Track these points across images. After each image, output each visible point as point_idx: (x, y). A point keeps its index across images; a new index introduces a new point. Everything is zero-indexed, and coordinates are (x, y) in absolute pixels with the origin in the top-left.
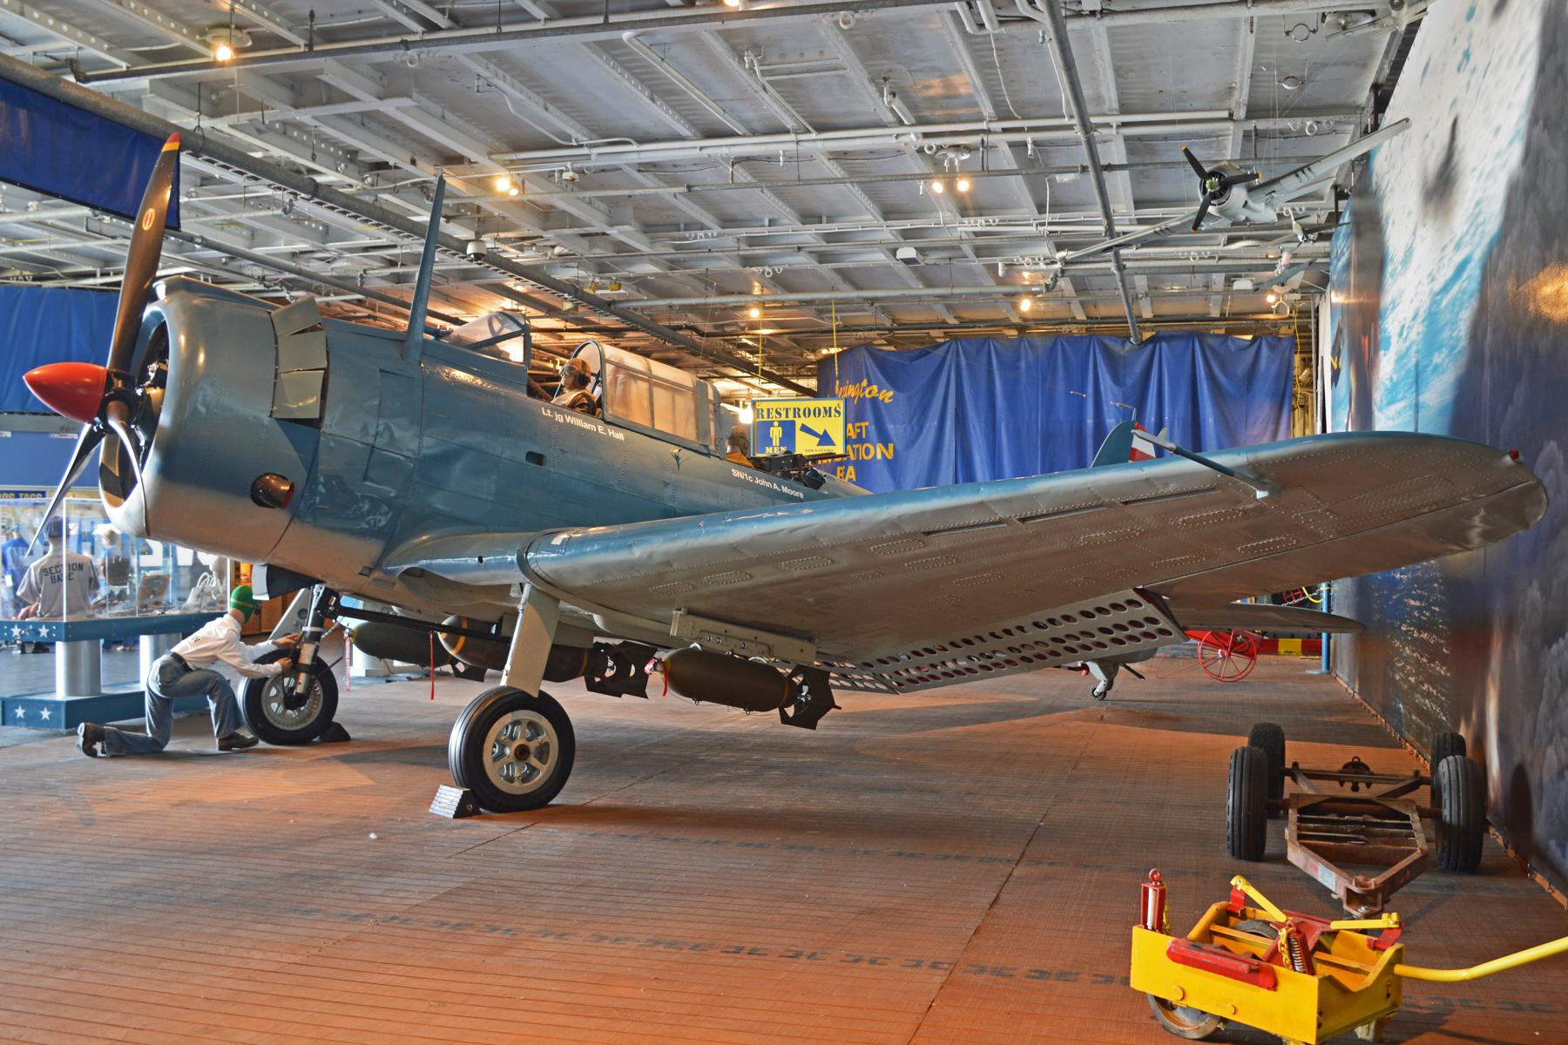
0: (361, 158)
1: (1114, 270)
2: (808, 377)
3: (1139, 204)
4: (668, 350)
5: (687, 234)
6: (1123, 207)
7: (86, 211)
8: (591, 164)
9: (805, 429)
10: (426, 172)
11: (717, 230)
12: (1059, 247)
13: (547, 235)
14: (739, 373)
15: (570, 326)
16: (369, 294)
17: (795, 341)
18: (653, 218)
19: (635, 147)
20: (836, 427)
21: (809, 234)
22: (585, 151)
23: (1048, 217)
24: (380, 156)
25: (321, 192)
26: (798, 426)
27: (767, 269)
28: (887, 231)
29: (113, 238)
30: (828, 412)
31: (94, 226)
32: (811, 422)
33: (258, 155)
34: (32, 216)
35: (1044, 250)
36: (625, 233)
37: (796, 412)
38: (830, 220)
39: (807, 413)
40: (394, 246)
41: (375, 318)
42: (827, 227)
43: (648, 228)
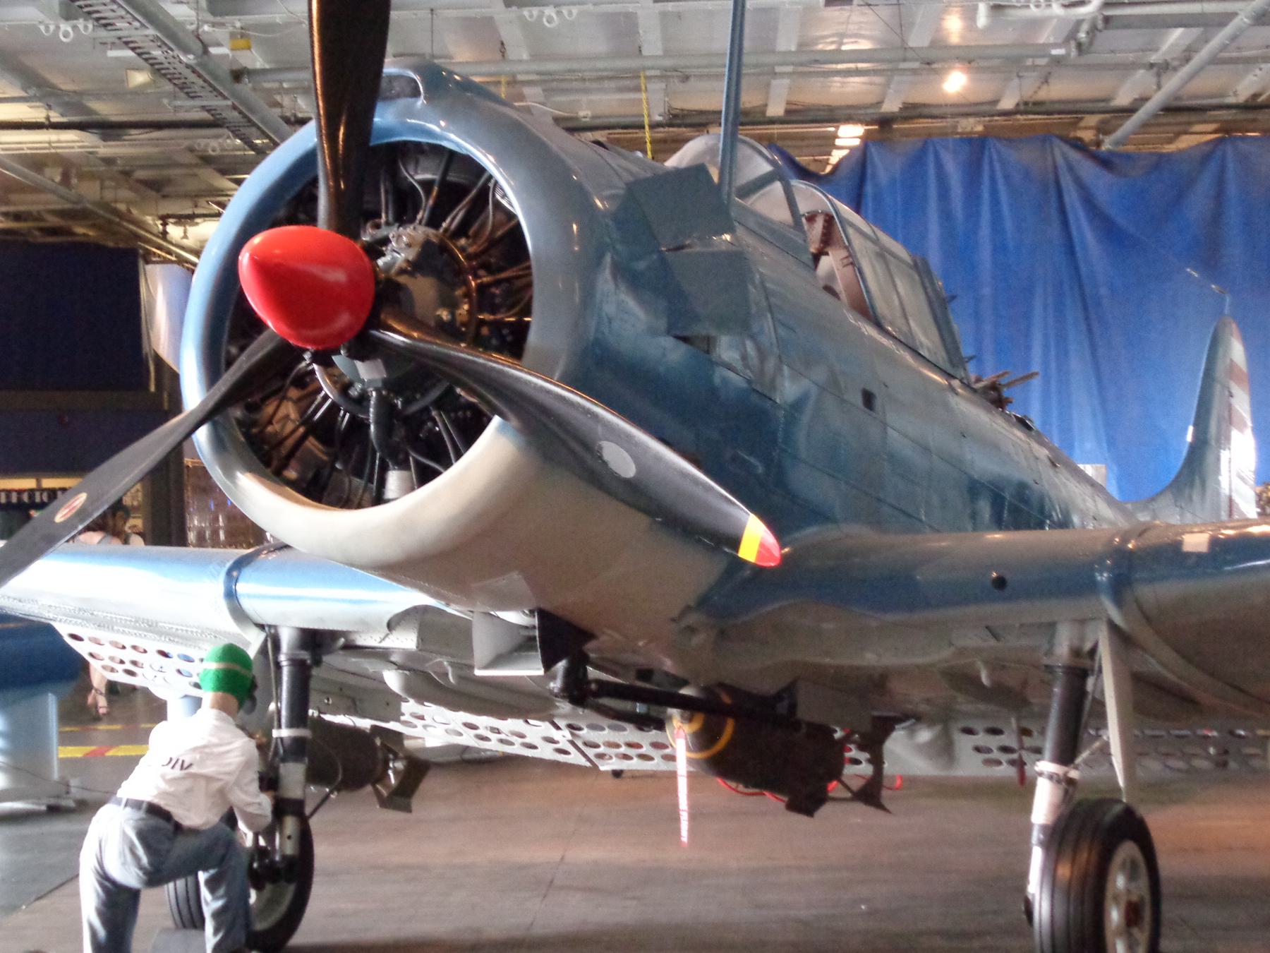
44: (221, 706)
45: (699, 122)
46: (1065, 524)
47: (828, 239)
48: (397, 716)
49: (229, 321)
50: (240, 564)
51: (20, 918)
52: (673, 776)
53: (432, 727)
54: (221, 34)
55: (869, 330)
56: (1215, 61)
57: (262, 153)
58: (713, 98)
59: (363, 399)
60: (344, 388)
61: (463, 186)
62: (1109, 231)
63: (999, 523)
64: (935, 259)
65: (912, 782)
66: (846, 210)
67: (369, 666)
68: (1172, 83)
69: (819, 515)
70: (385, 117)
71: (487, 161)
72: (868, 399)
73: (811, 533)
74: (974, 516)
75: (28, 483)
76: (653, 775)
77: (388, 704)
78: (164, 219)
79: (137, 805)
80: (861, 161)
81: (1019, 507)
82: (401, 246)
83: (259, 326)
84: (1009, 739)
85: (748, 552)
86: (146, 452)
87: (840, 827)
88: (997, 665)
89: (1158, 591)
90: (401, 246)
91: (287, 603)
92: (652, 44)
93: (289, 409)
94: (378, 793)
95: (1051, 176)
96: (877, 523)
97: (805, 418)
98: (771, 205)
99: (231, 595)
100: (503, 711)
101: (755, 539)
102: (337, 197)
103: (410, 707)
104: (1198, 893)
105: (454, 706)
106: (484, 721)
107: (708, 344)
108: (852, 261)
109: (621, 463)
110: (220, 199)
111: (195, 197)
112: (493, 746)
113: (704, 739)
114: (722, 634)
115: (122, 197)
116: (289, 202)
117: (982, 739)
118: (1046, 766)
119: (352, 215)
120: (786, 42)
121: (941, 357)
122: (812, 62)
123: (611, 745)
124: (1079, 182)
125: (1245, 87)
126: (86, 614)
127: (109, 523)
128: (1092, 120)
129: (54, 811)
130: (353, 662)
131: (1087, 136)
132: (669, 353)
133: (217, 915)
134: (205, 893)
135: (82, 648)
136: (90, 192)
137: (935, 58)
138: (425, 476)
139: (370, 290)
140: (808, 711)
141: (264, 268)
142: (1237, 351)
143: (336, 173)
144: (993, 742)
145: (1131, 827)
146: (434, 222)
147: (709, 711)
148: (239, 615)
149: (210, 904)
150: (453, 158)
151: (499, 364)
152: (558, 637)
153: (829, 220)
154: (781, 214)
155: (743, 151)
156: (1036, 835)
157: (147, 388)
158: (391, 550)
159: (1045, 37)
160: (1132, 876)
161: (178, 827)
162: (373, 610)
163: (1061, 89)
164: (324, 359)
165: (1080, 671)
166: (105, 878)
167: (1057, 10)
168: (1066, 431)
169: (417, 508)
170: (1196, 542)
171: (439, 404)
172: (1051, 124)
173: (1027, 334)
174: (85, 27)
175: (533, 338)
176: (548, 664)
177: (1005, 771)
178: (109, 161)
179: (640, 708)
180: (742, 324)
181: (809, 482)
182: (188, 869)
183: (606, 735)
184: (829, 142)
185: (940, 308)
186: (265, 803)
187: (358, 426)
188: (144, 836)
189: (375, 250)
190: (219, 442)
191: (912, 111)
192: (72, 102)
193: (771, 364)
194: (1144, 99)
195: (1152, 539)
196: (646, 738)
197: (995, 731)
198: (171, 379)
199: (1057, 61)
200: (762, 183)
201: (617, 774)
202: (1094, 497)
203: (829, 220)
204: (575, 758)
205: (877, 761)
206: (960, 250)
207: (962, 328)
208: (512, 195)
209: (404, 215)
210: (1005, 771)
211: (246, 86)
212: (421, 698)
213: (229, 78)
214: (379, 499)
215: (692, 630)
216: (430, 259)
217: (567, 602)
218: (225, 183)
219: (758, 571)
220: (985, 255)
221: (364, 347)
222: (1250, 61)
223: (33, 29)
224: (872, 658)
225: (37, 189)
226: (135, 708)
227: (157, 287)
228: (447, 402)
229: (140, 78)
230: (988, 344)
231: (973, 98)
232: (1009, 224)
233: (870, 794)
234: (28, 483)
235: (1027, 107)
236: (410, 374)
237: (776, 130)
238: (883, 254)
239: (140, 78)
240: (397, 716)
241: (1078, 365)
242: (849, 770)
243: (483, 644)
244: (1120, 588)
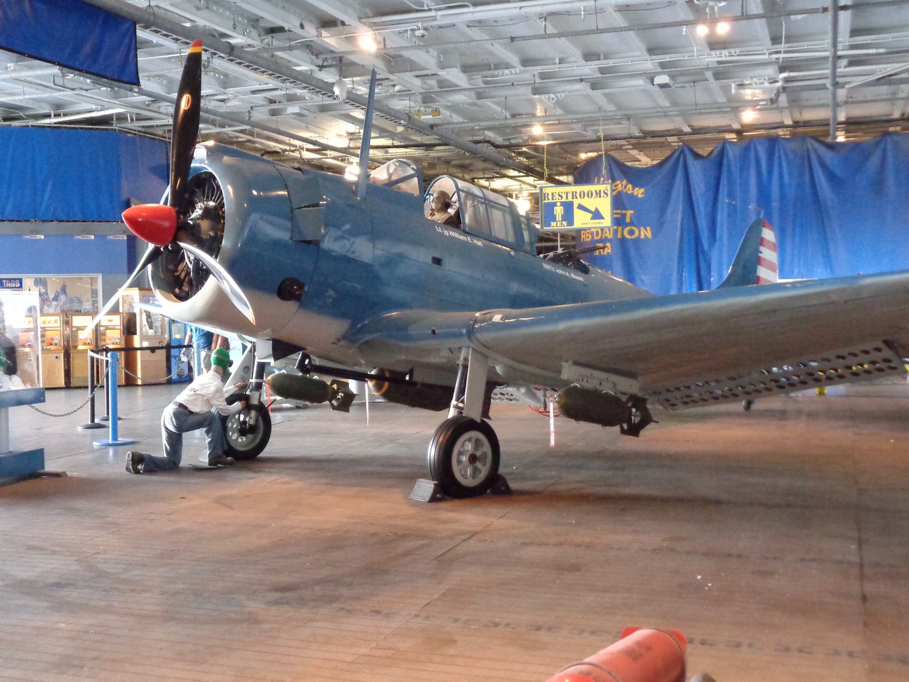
0: (262, 24)
1: (829, 86)
2: (567, 174)
3: (855, 32)
4: (466, 158)
5: (496, 72)
6: (844, 38)
7: (56, 70)
8: (435, 23)
9: (581, 207)
10: (310, 32)
11: (519, 68)
12: (782, 69)
13: (391, 77)
14: (516, 173)
15: (396, 143)
16: (254, 125)
17: (563, 149)
18: (470, 61)
19: (471, 9)
20: (605, 205)
21: (589, 69)
22: (432, 13)
23: (783, 47)
24: (279, 23)
25: (235, 53)
26: (575, 206)
27: (552, 96)
28: (649, 64)
29: (73, 89)
30: (598, 194)
31: (59, 81)
32: (586, 202)
33: (188, 25)
34: (14, 75)
35: (771, 71)
36: (455, 75)
37: (574, 195)
38: (607, 57)
39: (583, 194)
40: (277, 89)
41: (253, 142)
42: (603, 63)
43: (467, 69)
62: (832, 177)
94: (332, 405)
95: (806, 155)
124: (822, 164)
147: (379, 379)
161: (191, 413)
213: (429, 128)
231: (763, 122)
232: (786, 177)
241: (797, 239)
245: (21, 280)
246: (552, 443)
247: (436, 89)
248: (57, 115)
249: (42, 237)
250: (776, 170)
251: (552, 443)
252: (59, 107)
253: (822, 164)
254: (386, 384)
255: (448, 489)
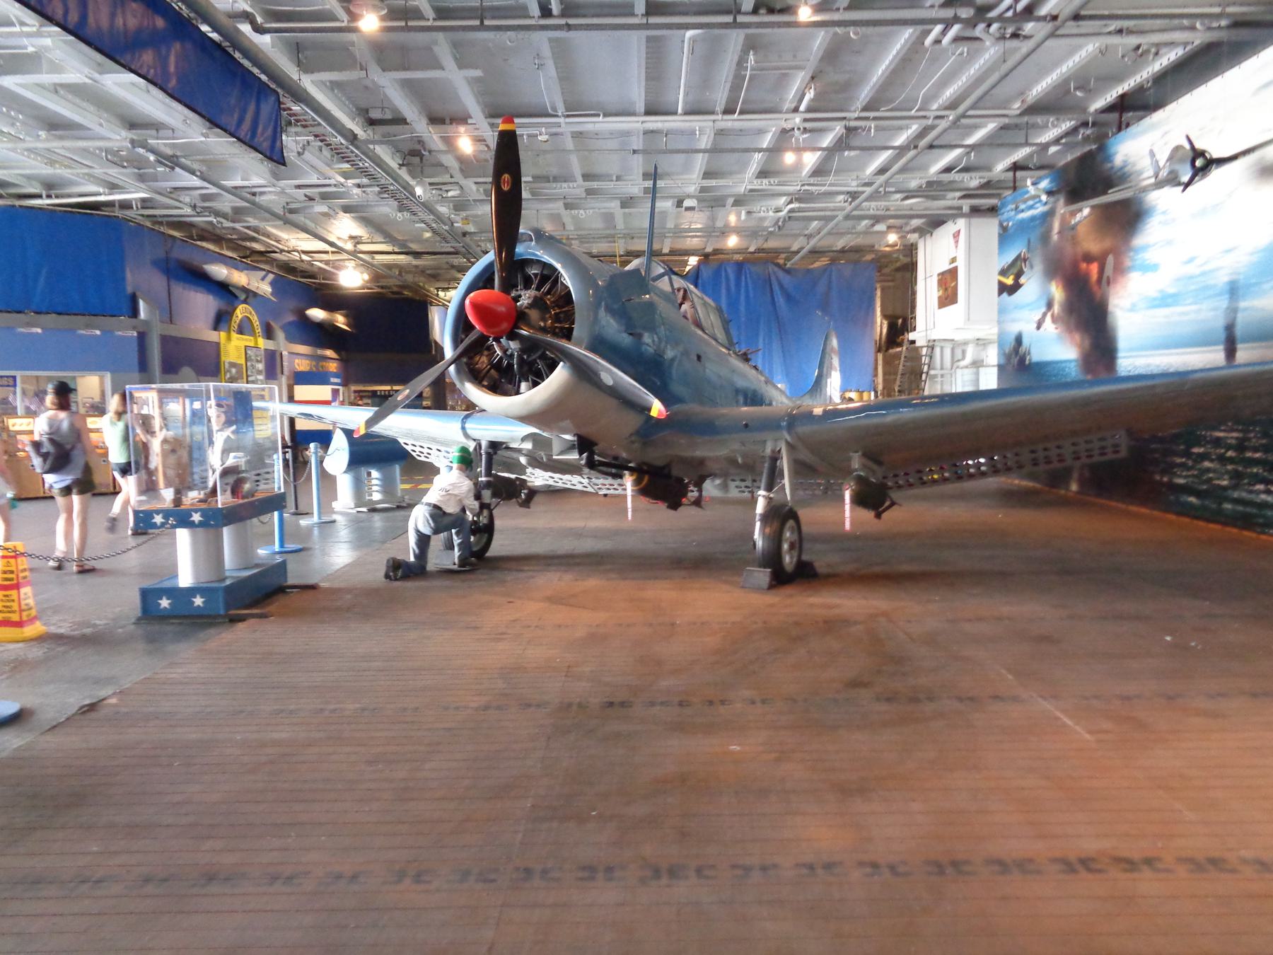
44: (460, 469)
45: (637, 255)
46: (770, 404)
47: (685, 298)
48: (525, 474)
49: (462, 326)
50: (466, 417)
51: (388, 545)
52: (625, 496)
53: (538, 478)
54: (458, 218)
55: (700, 332)
56: (829, 233)
57: (473, 264)
58: (642, 245)
59: (512, 355)
60: (505, 351)
61: (549, 275)
62: (789, 297)
63: (746, 404)
64: (724, 307)
65: (713, 499)
66: (692, 287)
67: (515, 455)
68: (813, 242)
69: (680, 400)
70: (520, 249)
71: (558, 266)
72: (699, 358)
73: (676, 407)
74: (737, 402)
75: (388, 388)
76: (618, 496)
77: (522, 469)
78: (438, 289)
79: (429, 504)
80: (697, 270)
81: (754, 398)
82: (526, 298)
83: (473, 327)
84: (748, 483)
85: (654, 413)
86: (432, 374)
87: (687, 513)
88: (744, 456)
89: (803, 429)
90: (526, 298)
91: (484, 432)
92: (620, 225)
93: (484, 359)
96: (702, 403)
97: (676, 364)
98: (664, 284)
99: (463, 428)
100: (563, 472)
101: (657, 408)
102: (502, 279)
103: (529, 470)
104: (816, 539)
105: (546, 470)
106: (557, 476)
107: (640, 336)
108: (693, 307)
109: (607, 380)
110: (458, 280)
111: (449, 281)
112: (560, 484)
113: (637, 482)
114: (645, 444)
115: (421, 281)
116: (484, 280)
117: (737, 483)
118: (762, 492)
119: (508, 286)
120: (670, 225)
121: (726, 342)
122: (679, 232)
123: (603, 484)
124: (781, 286)
125: (840, 244)
126: (409, 434)
127: (416, 403)
128: (783, 256)
129: (399, 507)
130: (509, 453)
131: (781, 262)
132: (625, 340)
133: (459, 545)
134: (455, 537)
135: (409, 448)
136: (409, 278)
137: (725, 232)
138: (535, 384)
139: (515, 314)
140: (675, 472)
141: (475, 305)
142: (834, 342)
143: (502, 270)
144: (743, 484)
145: (792, 515)
146: (538, 289)
147: (639, 472)
148: (467, 436)
149: (456, 541)
150: (545, 265)
151: (563, 343)
152: (584, 444)
153: (685, 291)
154: (667, 288)
155: (654, 264)
156: (758, 517)
157: (430, 351)
158: (523, 411)
159: (766, 224)
160: (792, 533)
162: (516, 434)
163: (772, 244)
164: (497, 340)
165: (775, 458)
166: (418, 531)
167: (771, 213)
168: (771, 371)
169: (532, 396)
170: (818, 411)
171: (540, 357)
172: (767, 257)
173: (757, 335)
174: (407, 215)
175: (575, 333)
176: (581, 454)
177: (747, 495)
178: (416, 267)
179: (614, 471)
180: (652, 329)
181: (677, 388)
182: (448, 529)
183: (601, 481)
184: (685, 263)
185: (726, 324)
186: (476, 505)
187: (510, 365)
188: (432, 516)
189: (517, 299)
190: (458, 371)
191: (717, 252)
192: (402, 244)
193: (663, 344)
194: (802, 248)
195: (802, 409)
196: (616, 482)
197: (743, 480)
198: (440, 350)
199: (771, 233)
200: (662, 275)
201: (605, 495)
202: (781, 396)
203: (685, 291)
204: (590, 489)
205: (700, 491)
206: (733, 304)
207: (734, 332)
208: (567, 279)
209: (527, 287)
210: (747, 495)
211: (467, 239)
212: (534, 467)
214: (518, 393)
215: (633, 442)
216: (537, 303)
217: (587, 431)
218: (459, 275)
219: (658, 421)
220: (742, 308)
221: (512, 336)
222: (842, 234)
223: (387, 216)
224: (699, 453)
225: (391, 277)
226: (429, 471)
227: (435, 315)
228: (543, 357)
229: (428, 235)
230: (742, 338)
232: (751, 295)
233: (698, 503)
234: (388, 388)
235: (759, 250)
236: (530, 346)
237: (666, 258)
238: (705, 304)
239: (428, 235)
240: (525, 474)
241: (776, 346)
242: (690, 494)
243: (556, 447)
244: (790, 427)
245: (14, 378)
246: (848, 526)
247: (584, 195)
248: (49, 196)
249: (39, 330)
250: (743, 290)
251: (848, 526)
252: (51, 186)
253: (781, 286)
254: (646, 479)
255: (781, 578)
